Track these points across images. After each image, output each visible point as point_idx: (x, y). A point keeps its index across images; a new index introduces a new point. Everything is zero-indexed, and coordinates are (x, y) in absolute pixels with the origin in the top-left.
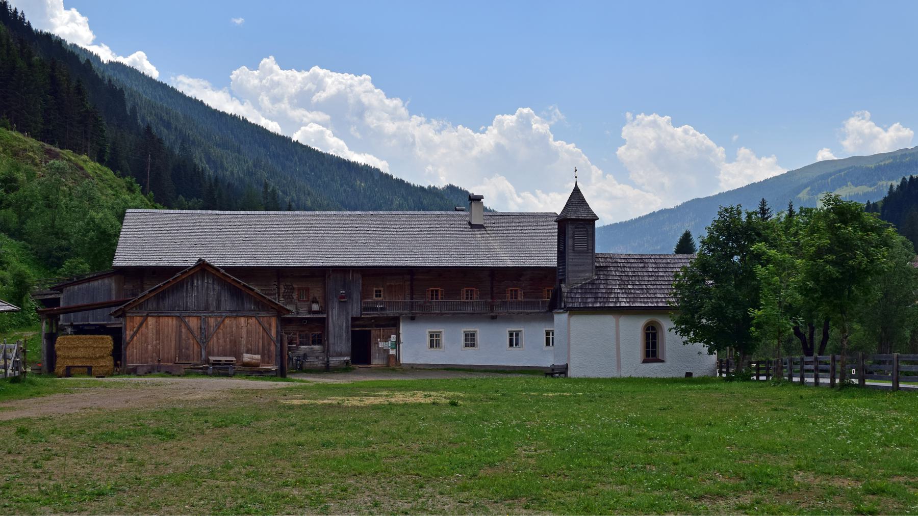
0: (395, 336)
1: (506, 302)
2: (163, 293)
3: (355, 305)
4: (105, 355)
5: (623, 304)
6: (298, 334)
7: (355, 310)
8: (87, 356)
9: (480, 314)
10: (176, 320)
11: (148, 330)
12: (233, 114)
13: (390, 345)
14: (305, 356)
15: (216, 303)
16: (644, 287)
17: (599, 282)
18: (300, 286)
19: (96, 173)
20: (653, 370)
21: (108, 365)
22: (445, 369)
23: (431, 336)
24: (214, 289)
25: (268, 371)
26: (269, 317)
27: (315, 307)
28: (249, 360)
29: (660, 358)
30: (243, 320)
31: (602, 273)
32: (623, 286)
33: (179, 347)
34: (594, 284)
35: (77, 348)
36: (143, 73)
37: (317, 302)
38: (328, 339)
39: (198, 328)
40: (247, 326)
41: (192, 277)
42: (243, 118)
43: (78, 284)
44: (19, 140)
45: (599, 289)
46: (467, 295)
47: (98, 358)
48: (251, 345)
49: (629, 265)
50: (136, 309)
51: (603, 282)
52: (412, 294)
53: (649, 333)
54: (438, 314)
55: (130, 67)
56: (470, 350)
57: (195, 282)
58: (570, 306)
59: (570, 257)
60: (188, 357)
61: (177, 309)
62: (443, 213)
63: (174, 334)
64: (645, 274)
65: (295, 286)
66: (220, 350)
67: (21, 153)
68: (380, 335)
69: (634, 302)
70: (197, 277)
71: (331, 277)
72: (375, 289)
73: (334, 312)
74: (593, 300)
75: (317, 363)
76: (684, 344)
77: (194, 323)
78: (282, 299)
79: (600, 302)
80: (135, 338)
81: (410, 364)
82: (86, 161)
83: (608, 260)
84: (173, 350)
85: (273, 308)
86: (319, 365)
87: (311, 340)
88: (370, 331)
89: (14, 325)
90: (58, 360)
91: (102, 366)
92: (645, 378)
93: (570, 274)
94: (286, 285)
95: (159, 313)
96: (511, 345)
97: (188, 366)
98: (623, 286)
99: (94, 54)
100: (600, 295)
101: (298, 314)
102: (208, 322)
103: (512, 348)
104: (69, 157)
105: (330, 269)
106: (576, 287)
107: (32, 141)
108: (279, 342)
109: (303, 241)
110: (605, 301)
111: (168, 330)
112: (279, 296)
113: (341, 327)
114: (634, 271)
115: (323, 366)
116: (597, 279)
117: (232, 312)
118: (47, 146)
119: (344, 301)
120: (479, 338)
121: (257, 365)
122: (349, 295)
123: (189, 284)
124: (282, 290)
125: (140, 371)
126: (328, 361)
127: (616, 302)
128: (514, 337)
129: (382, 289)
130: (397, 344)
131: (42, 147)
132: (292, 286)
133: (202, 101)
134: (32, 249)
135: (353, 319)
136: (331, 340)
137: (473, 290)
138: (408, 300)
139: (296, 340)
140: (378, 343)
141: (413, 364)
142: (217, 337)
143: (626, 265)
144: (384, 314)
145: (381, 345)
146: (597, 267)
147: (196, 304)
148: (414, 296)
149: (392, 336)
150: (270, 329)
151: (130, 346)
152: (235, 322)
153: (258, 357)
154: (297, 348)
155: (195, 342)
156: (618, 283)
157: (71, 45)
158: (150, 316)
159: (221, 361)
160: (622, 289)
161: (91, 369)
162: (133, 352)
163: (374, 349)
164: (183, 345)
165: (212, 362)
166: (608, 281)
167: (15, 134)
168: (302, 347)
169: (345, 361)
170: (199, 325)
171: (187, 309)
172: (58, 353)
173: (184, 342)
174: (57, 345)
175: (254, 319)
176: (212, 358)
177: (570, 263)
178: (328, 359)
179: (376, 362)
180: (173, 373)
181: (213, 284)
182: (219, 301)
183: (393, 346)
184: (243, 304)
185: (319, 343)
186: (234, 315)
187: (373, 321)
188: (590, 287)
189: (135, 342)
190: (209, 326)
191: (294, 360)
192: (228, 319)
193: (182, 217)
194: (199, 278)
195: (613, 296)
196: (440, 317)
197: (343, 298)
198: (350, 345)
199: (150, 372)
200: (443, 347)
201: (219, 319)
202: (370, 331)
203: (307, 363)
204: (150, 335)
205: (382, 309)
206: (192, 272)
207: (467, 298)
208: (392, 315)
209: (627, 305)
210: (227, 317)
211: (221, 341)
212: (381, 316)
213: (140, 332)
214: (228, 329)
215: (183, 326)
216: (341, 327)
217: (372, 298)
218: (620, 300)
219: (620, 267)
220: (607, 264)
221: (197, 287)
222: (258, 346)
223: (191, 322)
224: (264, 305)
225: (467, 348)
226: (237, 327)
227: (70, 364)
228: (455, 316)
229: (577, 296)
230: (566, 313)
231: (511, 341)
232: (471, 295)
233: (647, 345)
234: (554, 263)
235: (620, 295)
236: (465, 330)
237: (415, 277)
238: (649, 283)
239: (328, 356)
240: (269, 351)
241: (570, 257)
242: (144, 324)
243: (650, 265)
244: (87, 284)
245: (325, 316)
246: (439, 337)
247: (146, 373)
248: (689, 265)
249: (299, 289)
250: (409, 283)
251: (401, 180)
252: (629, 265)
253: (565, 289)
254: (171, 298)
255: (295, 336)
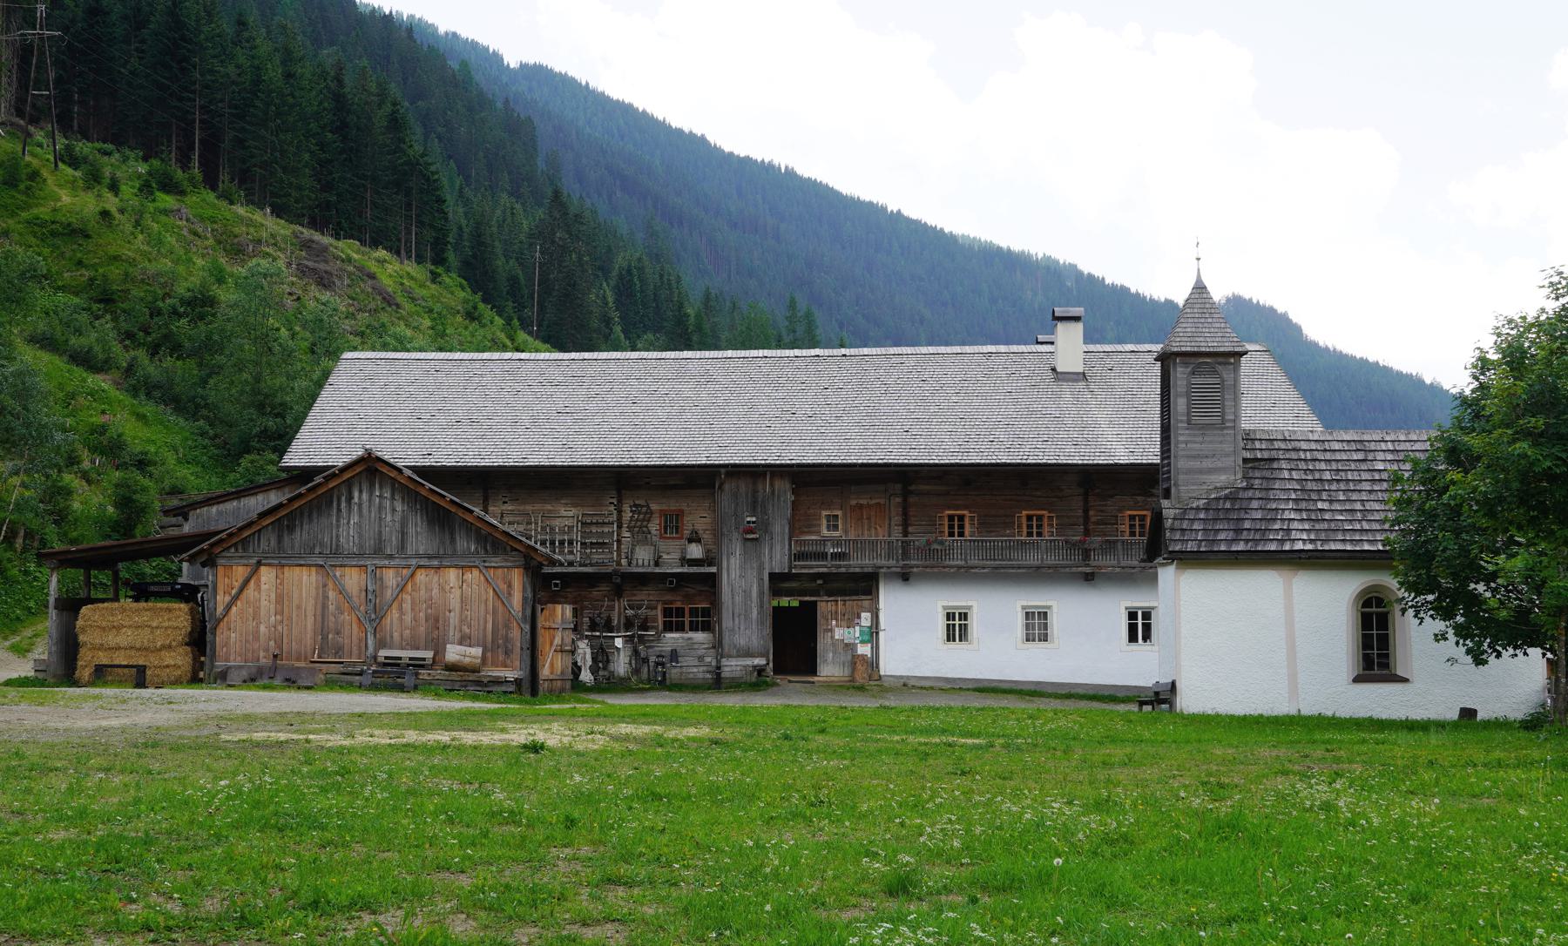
0: (869, 614)
1: (1115, 542)
2: (291, 516)
3: (778, 548)
4: (174, 644)
5: (1299, 546)
6: (659, 607)
7: (777, 557)
8: (138, 646)
9: (1055, 567)
10: (317, 573)
11: (259, 593)
12: (766, 161)
13: (857, 635)
14: (674, 655)
15: (397, 538)
16: (1358, 506)
17: (1250, 494)
18: (665, 507)
19: (402, 284)
20: (1379, 701)
21: (180, 663)
22: (975, 690)
23: (950, 616)
24: (394, 510)
25: (498, 682)
26: (507, 567)
27: (695, 551)
28: (458, 657)
29: (1400, 673)
30: (452, 575)
31: (1257, 474)
32: (1303, 505)
33: (322, 630)
34: (1236, 499)
35: (118, 628)
36: (587, 84)
37: (698, 540)
38: (720, 622)
39: (361, 590)
40: (461, 587)
41: (349, 484)
42: (787, 167)
43: (218, 503)
44: (250, 223)
45: (1246, 510)
46: (1030, 527)
47: (160, 650)
48: (470, 626)
49: (1328, 456)
50: (237, 550)
51: (1258, 495)
52: (905, 525)
53: (1370, 614)
54: (959, 567)
55: (560, 73)
56: (1037, 648)
57: (356, 494)
58: (1177, 548)
59: (1181, 438)
60: (339, 650)
61: (317, 550)
62: (1002, 348)
63: (312, 602)
64: (1365, 476)
65: (654, 507)
66: (404, 635)
67: (251, 248)
68: (836, 612)
69: (1325, 541)
70: (360, 484)
71: (727, 487)
72: (824, 513)
73: (732, 560)
74: (1231, 535)
75: (695, 670)
76: (1438, 641)
77: (353, 579)
78: (628, 534)
79: (1247, 541)
80: (234, 609)
81: (902, 677)
82: (385, 261)
83: (1277, 445)
84: (310, 634)
85: (516, 550)
86: (701, 676)
87: (687, 620)
88: (815, 603)
89: (105, 584)
90: (82, 651)
91: (167, 666)
92: (1371, 719)
93: (1181, 477)
94: (635, 505)
95: (282, 559)
96: (1133, 638)
97: (339, 668)
98: (1303, 505)
99: (491, 51)
100: (1247, 525)
101: (657, 564)
102: (381, 579)
103: (1133, 646)
104: (348, 255)
105: (723, 470)
106: (1194, 505)
107: (278, 224)
108: (529, 619)
109: (682, 410)
110: (1257, 537)
111: (301, 594)
112: (620, 527)
113: (747, 593)
114: (1338, 470)
115: (709, 676)
116: (1244, 489)
117: (430, 557)
118: (307, 233)
119: (754, 537)
120: (1055, 621)
121: (475, 670)
122: (764, 526)
123: (343, 498)
124: (627, 515)
125: (234, 677)
126: (719, 668)
127: (1282, 541)
128: (1140, 621)
129: (839, 513)
130: (873, 633)
131: (294, 234)
132: (648, 506)
133: (703, 135)
134: (216, 436)
135: (772, 576)
136: (727, 622)
137: (1043, 516)
138: (897, 534)
139: (655, 620)
140: (831, 630)
141: (908, 677)
142: (400, 609)
143: (1320, 456)
144: (840, 566)
145: (839, 633)
146: (1245, 460)
147: (357, 541)
148: (910, 529)
149: (863, 615)
150: (510, 594)
151: (223, 625)
152: (436, 578)
153: (477, 652)
154: (658, 638)
155: (354, 618)
156: (1293, 496)
157: (447, 34)
158: (265, 565)
159: (400, 658)
160: (1301, 510)
161: (144, 672)
162: (230, 641)
163: (823, 642)
164: (331, 625)
165: (383, 660)
166: (1271, 492)
167: (241, 210)
168: (669, 635)
169: (754, 667)
170: (364, 584)
171: (337, 552)
172: (82, 638)
173: (332, 619)
174: (79, 623)
175: (476, 572)
176: (383, 653)
177: (1181, 453)
178: (718, 661)
179: (830, 669)
180: (301, 683)
181: (393, 498)
182: (403, 534)
183: (866, 638)
184: (453, 540)
185: (706, 627)
186: (436, 563)
187: (820, 582)
188: (1228, 505)
189: (233, 618)
190: (383, 587)
191: (652, 664)
192: (423, 570)
193: (448, 366)
194: (364, 488)
195: (1277, 527)
196: (965, 575)
197: (751, 531)
198: (768, 631)
199: (253, 680)
200: (975, 641)
201: (405, 571)
202: (815, 603)
203: (674, 671)
204: (264, 603)
205: (835, 556)
206: (347, 476)
207: (1030, 534)
208: (857, 570)
209: (1309, 547)
210: (420, 567)
211: (408, 618)
212: (834, 570)
213: (243, 596)
214: (423, 592)
215: (331, 585)
216: (747, 593)
217: (818, 533)
218: (1294, 535)
219: (1305, 460)
220: (1274, 454)
221: (360, 505)
222: (485, 627)
223: (347, 578)
224: (494, 543)
225: (1030, 644)
226: (442, 589)
227: (105, 661)
228: (1002, 573)
229: (1195, 526)
230: (1172, 563)
231: (1132, 630)
232: (1039, 526)
233: (1366, 643)
234: (1149, 453)
235: (1295, 525)
236: (1025, 603)
237: (913, 488)
238: (1372, 497)
239: (720, 656)
240: (507, 639)
241: (1181, 438)
242: (252, 582)
243: (1380, 456)
244: (235, 503)
245: (713, 570)
246: (966, 619)
247: (245, 681)
248: (1422, 456)
249: (663, 513)
250: (898, 500)
251: (1122, 286)
252: (1328, 456)
253: (1169, 510)
254: (306, 527)
255: (654, 613)
